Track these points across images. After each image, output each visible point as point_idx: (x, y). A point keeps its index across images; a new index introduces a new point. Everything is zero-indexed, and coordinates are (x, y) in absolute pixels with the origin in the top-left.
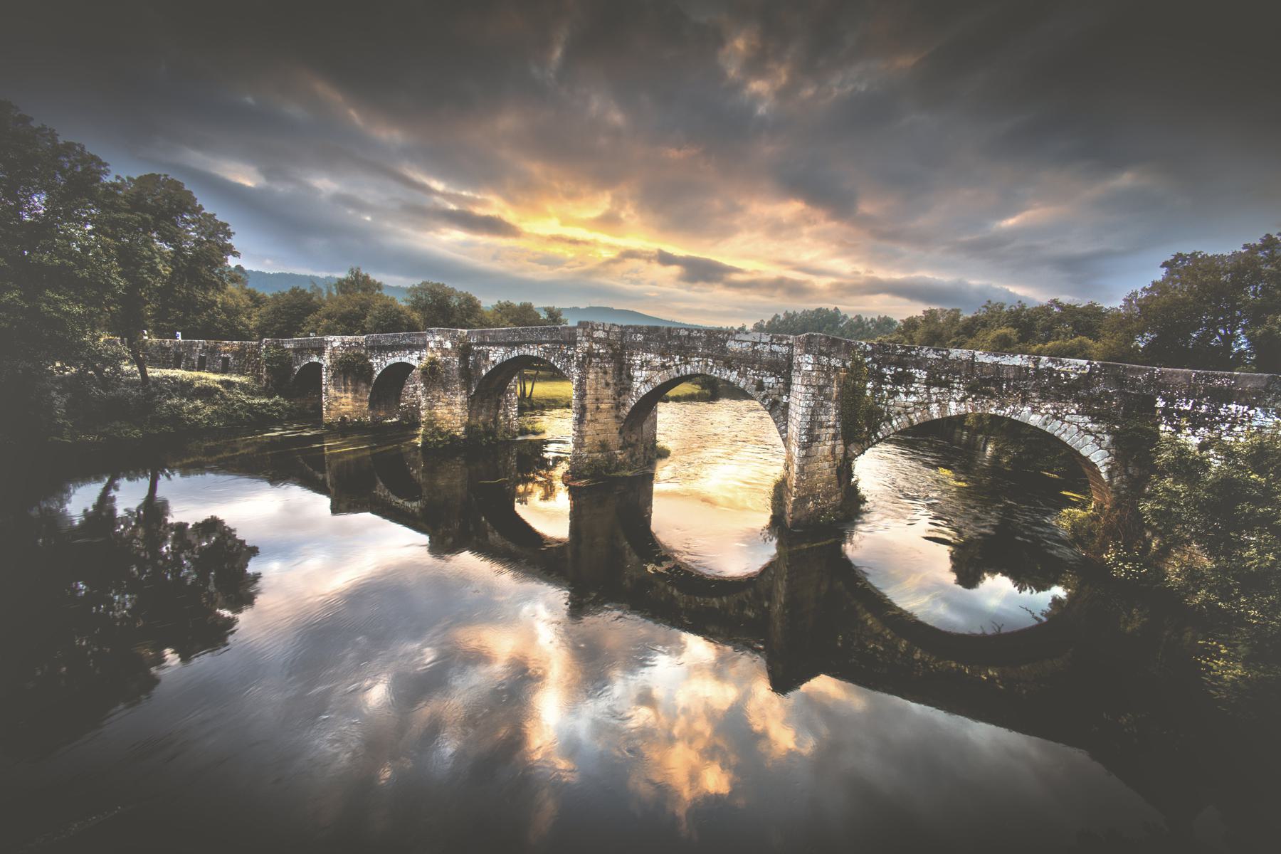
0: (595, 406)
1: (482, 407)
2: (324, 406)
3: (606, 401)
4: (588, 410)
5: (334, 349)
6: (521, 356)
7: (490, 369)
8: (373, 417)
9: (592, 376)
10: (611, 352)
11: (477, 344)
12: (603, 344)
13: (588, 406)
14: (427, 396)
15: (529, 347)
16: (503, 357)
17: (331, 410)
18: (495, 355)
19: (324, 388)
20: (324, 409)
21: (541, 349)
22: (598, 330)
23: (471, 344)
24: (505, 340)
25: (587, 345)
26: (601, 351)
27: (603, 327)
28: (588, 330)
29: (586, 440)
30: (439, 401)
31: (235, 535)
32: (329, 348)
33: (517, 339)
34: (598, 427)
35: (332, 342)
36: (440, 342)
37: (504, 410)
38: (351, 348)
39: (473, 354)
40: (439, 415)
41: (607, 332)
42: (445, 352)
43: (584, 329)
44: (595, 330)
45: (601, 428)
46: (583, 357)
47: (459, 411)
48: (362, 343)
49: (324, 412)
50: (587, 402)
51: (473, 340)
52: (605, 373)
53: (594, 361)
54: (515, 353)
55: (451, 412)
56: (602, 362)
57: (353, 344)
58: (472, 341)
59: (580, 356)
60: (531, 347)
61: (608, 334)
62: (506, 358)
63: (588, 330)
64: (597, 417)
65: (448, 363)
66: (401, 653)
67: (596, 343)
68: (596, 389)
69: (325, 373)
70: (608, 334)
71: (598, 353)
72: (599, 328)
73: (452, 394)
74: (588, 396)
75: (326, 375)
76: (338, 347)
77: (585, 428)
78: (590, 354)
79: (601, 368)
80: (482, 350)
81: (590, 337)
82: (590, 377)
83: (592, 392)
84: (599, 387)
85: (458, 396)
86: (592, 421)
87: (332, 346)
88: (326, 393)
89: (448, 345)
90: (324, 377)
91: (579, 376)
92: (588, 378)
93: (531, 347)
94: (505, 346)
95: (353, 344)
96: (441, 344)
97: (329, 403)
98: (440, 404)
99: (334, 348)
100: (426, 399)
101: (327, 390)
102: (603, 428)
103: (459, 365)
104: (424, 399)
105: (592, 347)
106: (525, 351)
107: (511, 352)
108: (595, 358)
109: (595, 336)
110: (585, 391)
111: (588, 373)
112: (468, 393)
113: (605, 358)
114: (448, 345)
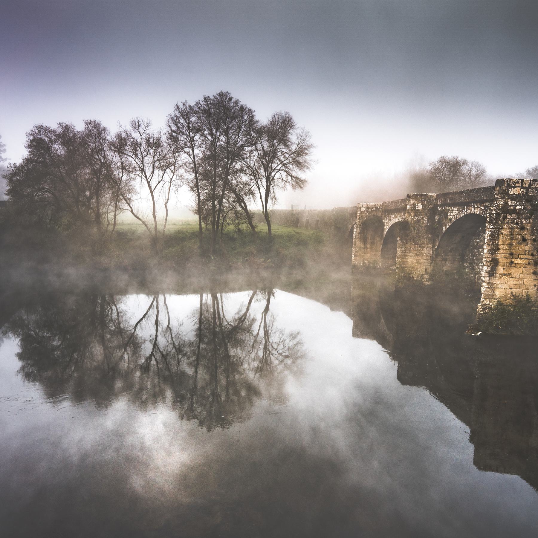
0: (508, 261)
1: (446, 260)
2: (353, 254)
3: (522, 256)
4: (500, 264)
5: (362, 213)
6: (469, 214)
7: (448, 227)
8: (383, 263)
9: (506, 231)
10: (530, 207)
11: (441, 206)
12: (521, 200)
13: (500, 260)
14: (402, 248)
15: (474, 207)
16: (456, 216)
17: (357, 256)
18: (452, 214)
19: (354, 241)
20: (353, 256)
21: (482, 207)
22: (515, 187)
23: (438, 205)
24: (459, 201)
25: (502, 202)
26: (518, 207)
27: (522, 184)
28: (504, 188)
29: (497, 293)
30: (410, 252)
31: (151, 296)
32: (359, 212)
33: (467, 200)
34: (512, 281)
35: (361, 207)
36: (414, 205)
37: (470, 263)
38: (372, 211)
39: (439, 214)
40: (410, 263)
41: (527, 189)
42: (417, 213)
43: (500, 187)
44: (511, 187)
45: (515, 283)
46: (497, 214)
47: (424, 261)
48: (380, 207)
49: (353, 258)
50: (499, 256)
51: (439, 202)
52: (522, 228)
53: (509, 217)
54: (465, 212)
55: (418, 262)
56: (518, 218)
57: (374, 209)
58: (438, 203)
59: (494, 212)
60: (476, 206)
61: (527, 191)
62: (458, 217)
63: (504, 188)
64: (510, 272)
65: (418, 222)
66: (117, 350)
67: (512, 200)
68: (510, 245)
69: (355, 230)
70: (527, 191)
71: (515, 209)
72: (517, 185)
73: (420, 247)
74: (501, 251)
75: (356, 232)
76: (364, 211)
77: (496, 281)
78: (505, 210)
79: (517, 223)
80: (444, 210)
81: (505, 194)
82: (504, 232)
83: (506, 247)
84: (514, 242)
85: (425, 249)
86: (505, 275)
87: (361, 211)
88: (355, 244)
89: (420, 207)
90: (354, 233)
91: (491, 231)
92: (502, 234)
93: (476, 206)
94: (458, 206)
95: (374, 209)
96: (415, 207)
97: (356, 252)
98: (411, 254)
99: (362, 212)
100: (401, 250)
101: (355, 242)
102: (519, 282)
103: (427, 223)
104: (399, 250)
105: (507, 203)
106: (471, 210)
107: (462, 211)
108: (510, 214)
109: (511, 193)
110: (498, 245)
111: (502, 228)
112: (433, 247)
113: (522, 214)
114: (420, 207)
